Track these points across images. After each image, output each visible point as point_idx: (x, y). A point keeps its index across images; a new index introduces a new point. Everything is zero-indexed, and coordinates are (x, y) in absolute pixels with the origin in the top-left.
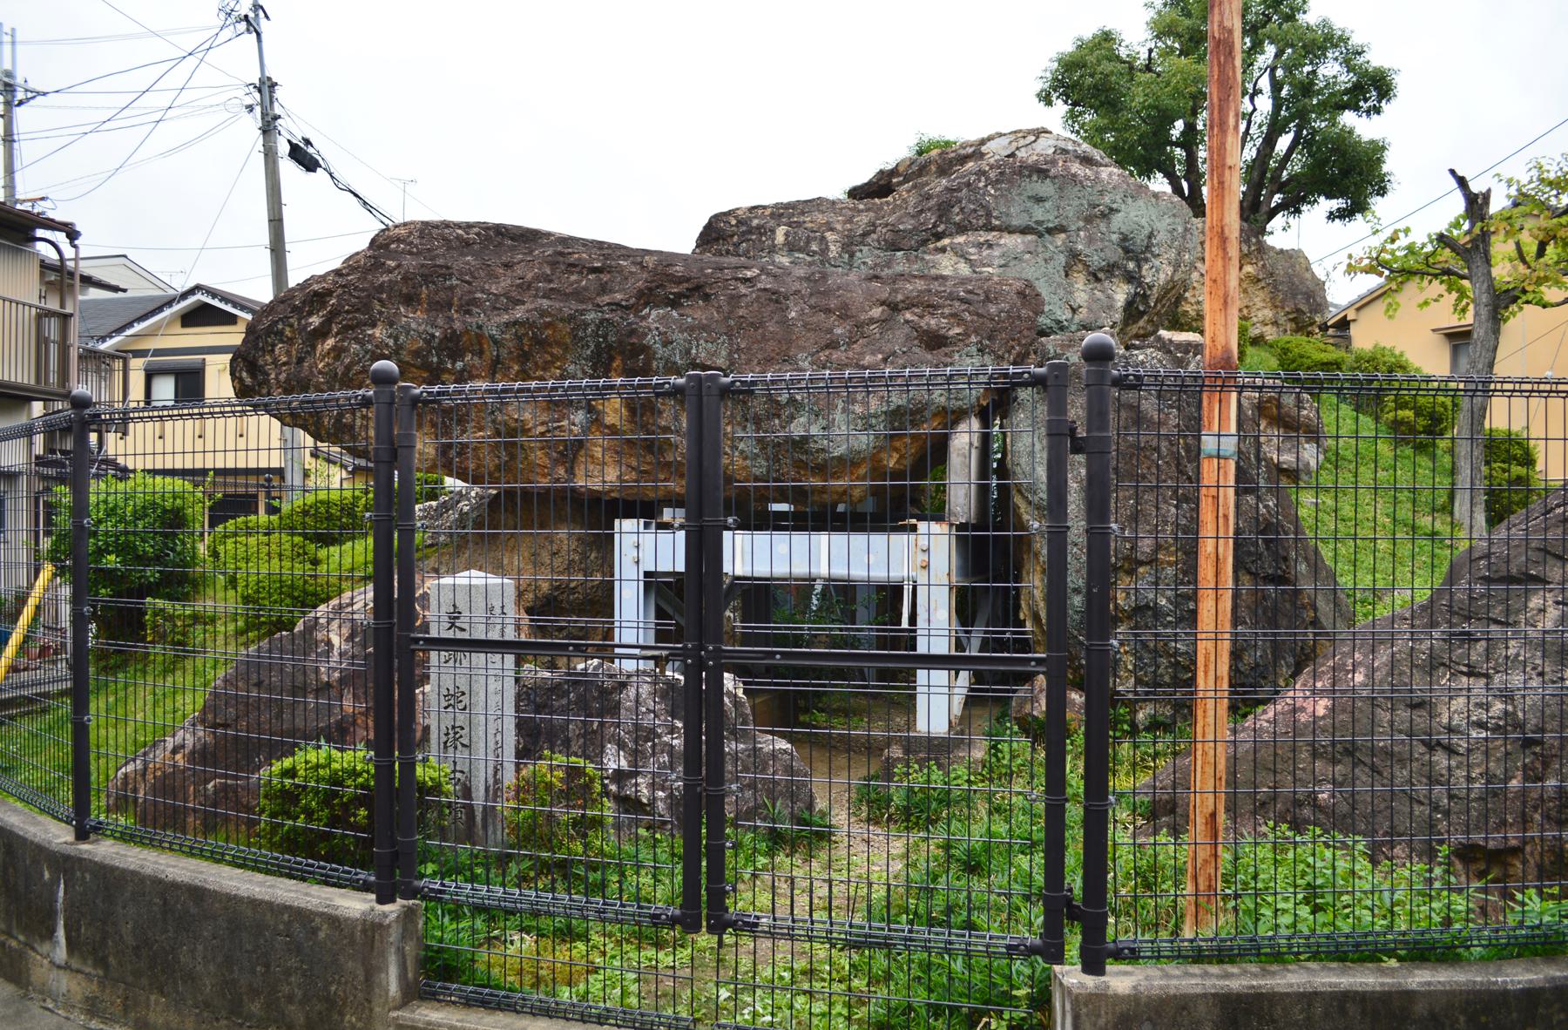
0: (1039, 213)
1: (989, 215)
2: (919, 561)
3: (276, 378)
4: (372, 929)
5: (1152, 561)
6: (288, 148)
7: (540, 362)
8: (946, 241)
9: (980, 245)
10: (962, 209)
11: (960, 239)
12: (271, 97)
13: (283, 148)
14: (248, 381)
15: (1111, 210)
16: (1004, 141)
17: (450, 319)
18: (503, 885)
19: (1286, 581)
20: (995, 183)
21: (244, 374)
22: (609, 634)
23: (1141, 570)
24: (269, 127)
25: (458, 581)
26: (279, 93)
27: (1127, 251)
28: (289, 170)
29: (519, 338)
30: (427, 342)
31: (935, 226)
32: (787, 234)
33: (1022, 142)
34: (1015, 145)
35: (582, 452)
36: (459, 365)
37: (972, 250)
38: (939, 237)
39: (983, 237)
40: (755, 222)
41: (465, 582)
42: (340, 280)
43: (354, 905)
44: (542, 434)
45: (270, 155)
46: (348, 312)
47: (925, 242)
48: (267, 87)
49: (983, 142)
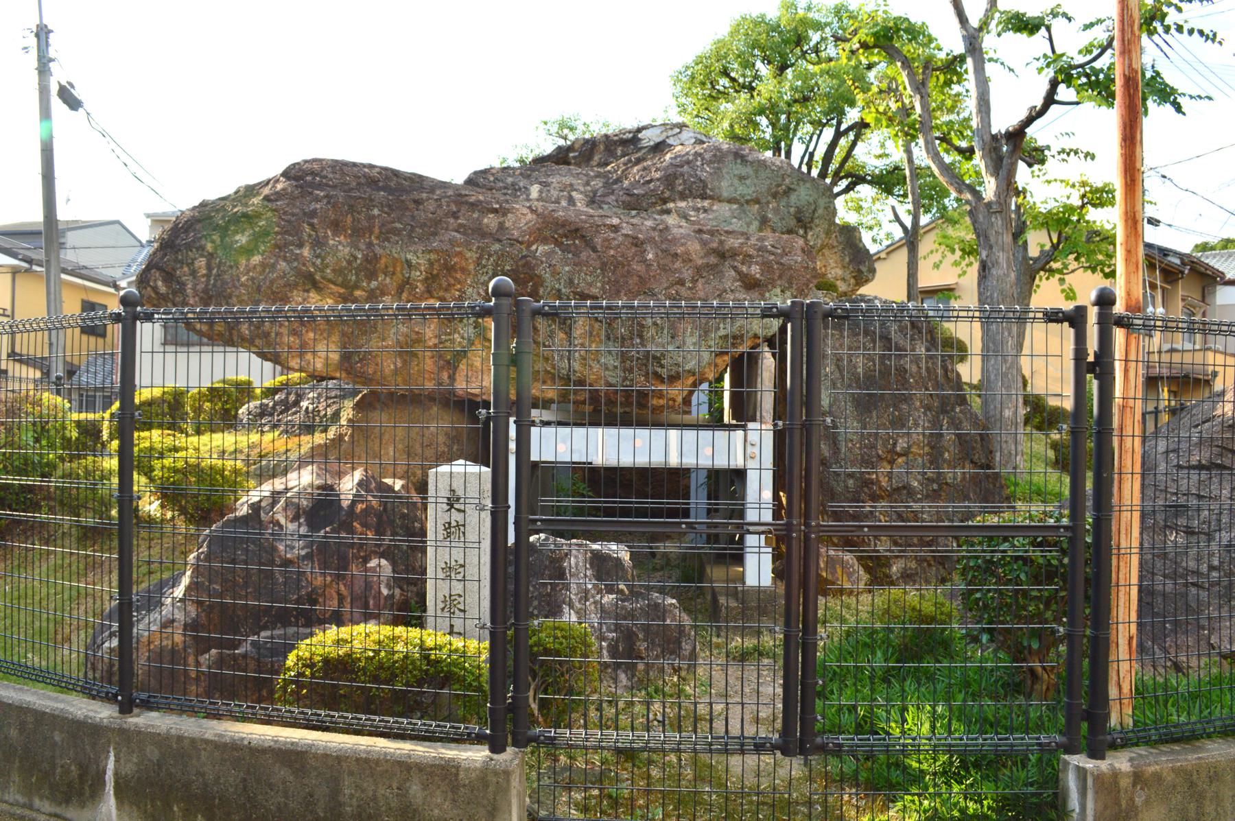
0: (742, 190)
1: (705, 186)
2: (750, 450)
3: (194, 289)
4: (485, 774)
5: (905, 453)
6: (57, 87)
7: (444, 284)
8: (671, 205)
9: (698, 210)
10: (685, 181)
11: (683, 204)
12: (47, 42)
13: (54, 89)
14: (163, 290)
15: (790, 189)
16: (657, 131)
17: (370, 245)
18: (585, 727)
19: (989, 467)
20: (710, 163)
21: (160, 283)
22: (741, 514)
23: (900, 460)
24: (44, 67)
25: (455, 469)
26: (52, 38)
27: (799, 220)
28: (57, 104)
29: (431, 263)
30: (349, 263)
31: (663, 193)
32: (541, 192)
33: (670, 133)
34: (665, 134)
35: (464, 361)
36: (374, 284)
37: (692, 213)
38: (665, 201)
39: (700, 203)
40: (510, 180)
41: (462, 469)
42: (270, 205)
43: (477, 755)
44: (435, 346)
45: (44, 91)
46: (277, 233)
47: (654, 204)
48: (42, 33)
49: (639, 130)
